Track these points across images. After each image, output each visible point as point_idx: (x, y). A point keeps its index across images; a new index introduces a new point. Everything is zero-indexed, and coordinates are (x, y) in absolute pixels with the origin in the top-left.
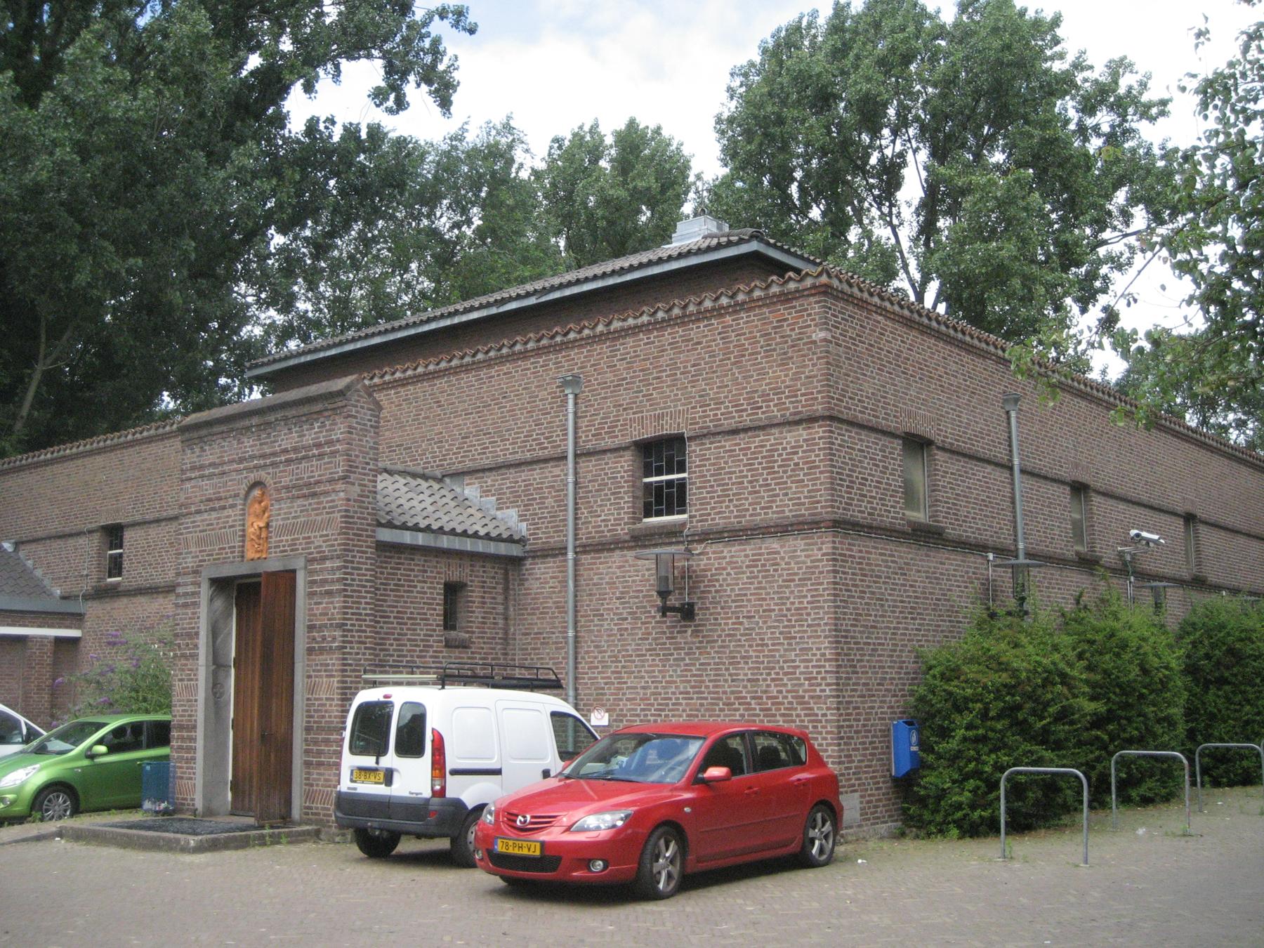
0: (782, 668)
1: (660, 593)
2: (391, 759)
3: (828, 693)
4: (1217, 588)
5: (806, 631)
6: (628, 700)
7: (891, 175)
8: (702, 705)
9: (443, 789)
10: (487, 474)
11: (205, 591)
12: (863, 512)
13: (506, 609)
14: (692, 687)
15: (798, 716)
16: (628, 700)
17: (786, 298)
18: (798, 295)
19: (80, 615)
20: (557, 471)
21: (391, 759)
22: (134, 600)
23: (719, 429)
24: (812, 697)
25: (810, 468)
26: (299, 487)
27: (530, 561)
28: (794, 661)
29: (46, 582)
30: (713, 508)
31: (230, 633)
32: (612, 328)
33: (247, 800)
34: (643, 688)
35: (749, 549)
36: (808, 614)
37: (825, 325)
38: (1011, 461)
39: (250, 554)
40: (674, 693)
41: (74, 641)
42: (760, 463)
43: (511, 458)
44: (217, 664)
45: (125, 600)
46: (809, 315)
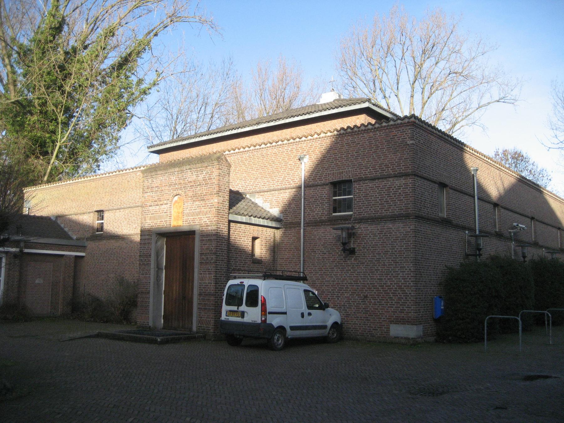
2: (243, 308)
4: (542, 247)
9: (266, 319)
14: (354, 281)
19: (85, 247)
21: (243, 308)
22: (109, 241)
24: (405, 286)
29: (70, 233)
31: (163, 256)
36: (404, 253)
37: (412, 138)
45: (105, 241)
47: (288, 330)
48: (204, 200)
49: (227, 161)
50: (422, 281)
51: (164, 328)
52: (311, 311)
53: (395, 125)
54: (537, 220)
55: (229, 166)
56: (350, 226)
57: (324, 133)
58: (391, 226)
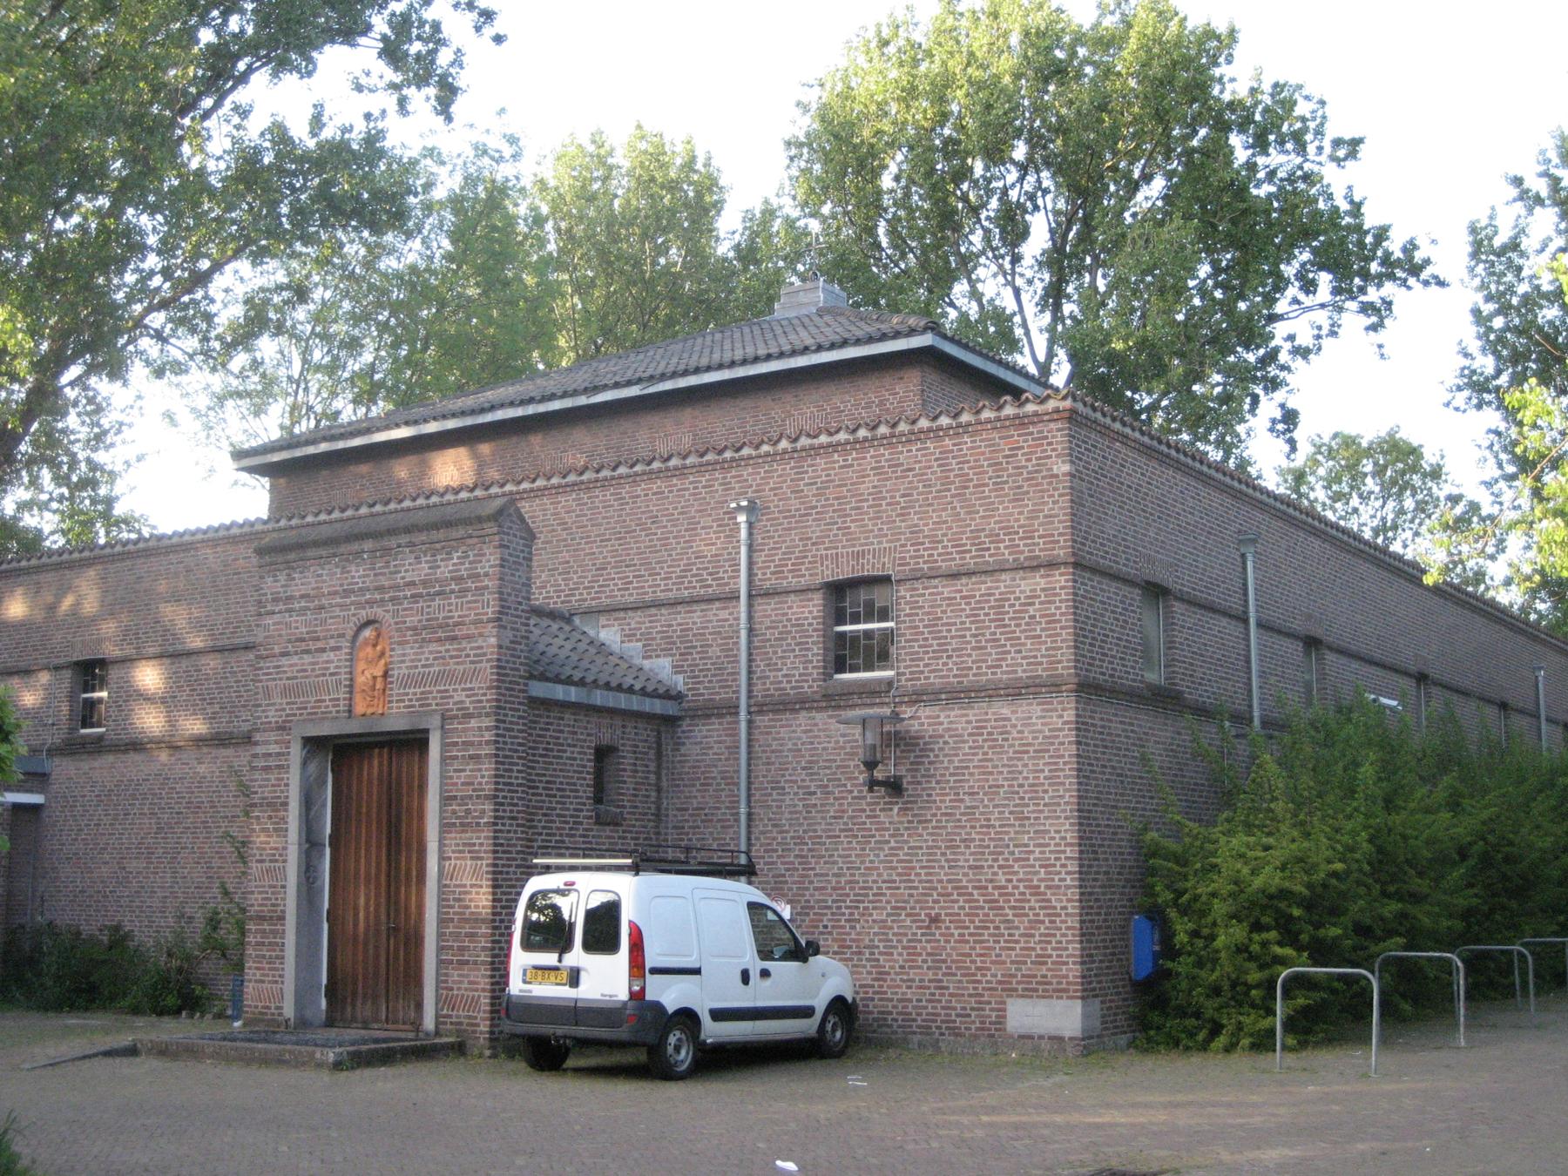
0: (1013, 853)
1: (866, 764)
2: (577, 956)
3: (1068, 882)
5: (1041, 811)
6: (816, 889)
7: (1013, 227)
8: (911, 895)
9: (643, 989)
10: (630, 613)
11: (296, 752)
12: (1103, 674)
13: (659, 778)
14: (899, 875)
15: (1031, 908)
16: (816, 889)
17: (1021, 422)
18: (1037, 418)
19: (44, 775)
20: (724, 614)
21: (577, 956)
22: (123, 757)
23: (934, 573)
24: (1048, 887)
25: (1048, 622)
26: (433, 629)
27: (688, 721)
28: (1026, 845)
30: (926, 665)
31: (324, 805)
32: (798, 445)
33: (349, 1009)
34: (835, 875)
35: (973, 714)
36: (1046, 791)
38: (1246, 612)
39: (360, 708)
40: (875, 882)
41: (35, 809)
42: (987, 615)
43: (662, 596)
44: (311, 843)
45: (111, 758)
46: (1050, 444)
47: (706, 1019)
48: (454, 638)
49: (522, 519)
50: (1097, 873)
51: (330, 1022)
52: (768, 965)
53: (1017, 417)
54: (1436, 683)
55: (531, 536)
56: (887, 711)
57: (809, 435)
58: (1006, 711)
